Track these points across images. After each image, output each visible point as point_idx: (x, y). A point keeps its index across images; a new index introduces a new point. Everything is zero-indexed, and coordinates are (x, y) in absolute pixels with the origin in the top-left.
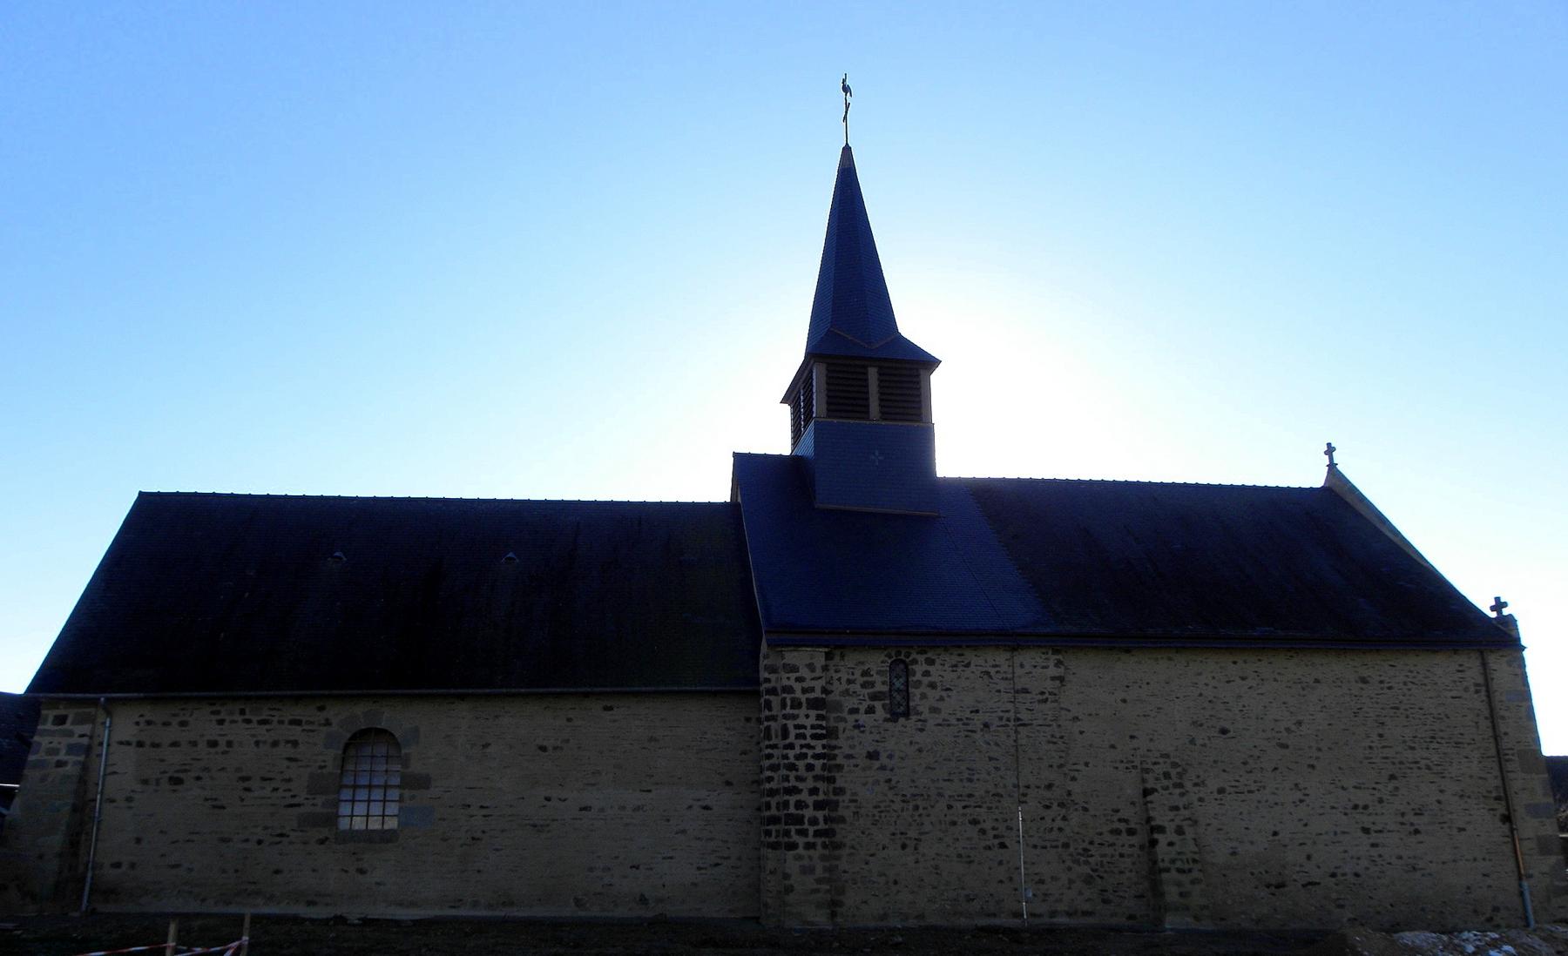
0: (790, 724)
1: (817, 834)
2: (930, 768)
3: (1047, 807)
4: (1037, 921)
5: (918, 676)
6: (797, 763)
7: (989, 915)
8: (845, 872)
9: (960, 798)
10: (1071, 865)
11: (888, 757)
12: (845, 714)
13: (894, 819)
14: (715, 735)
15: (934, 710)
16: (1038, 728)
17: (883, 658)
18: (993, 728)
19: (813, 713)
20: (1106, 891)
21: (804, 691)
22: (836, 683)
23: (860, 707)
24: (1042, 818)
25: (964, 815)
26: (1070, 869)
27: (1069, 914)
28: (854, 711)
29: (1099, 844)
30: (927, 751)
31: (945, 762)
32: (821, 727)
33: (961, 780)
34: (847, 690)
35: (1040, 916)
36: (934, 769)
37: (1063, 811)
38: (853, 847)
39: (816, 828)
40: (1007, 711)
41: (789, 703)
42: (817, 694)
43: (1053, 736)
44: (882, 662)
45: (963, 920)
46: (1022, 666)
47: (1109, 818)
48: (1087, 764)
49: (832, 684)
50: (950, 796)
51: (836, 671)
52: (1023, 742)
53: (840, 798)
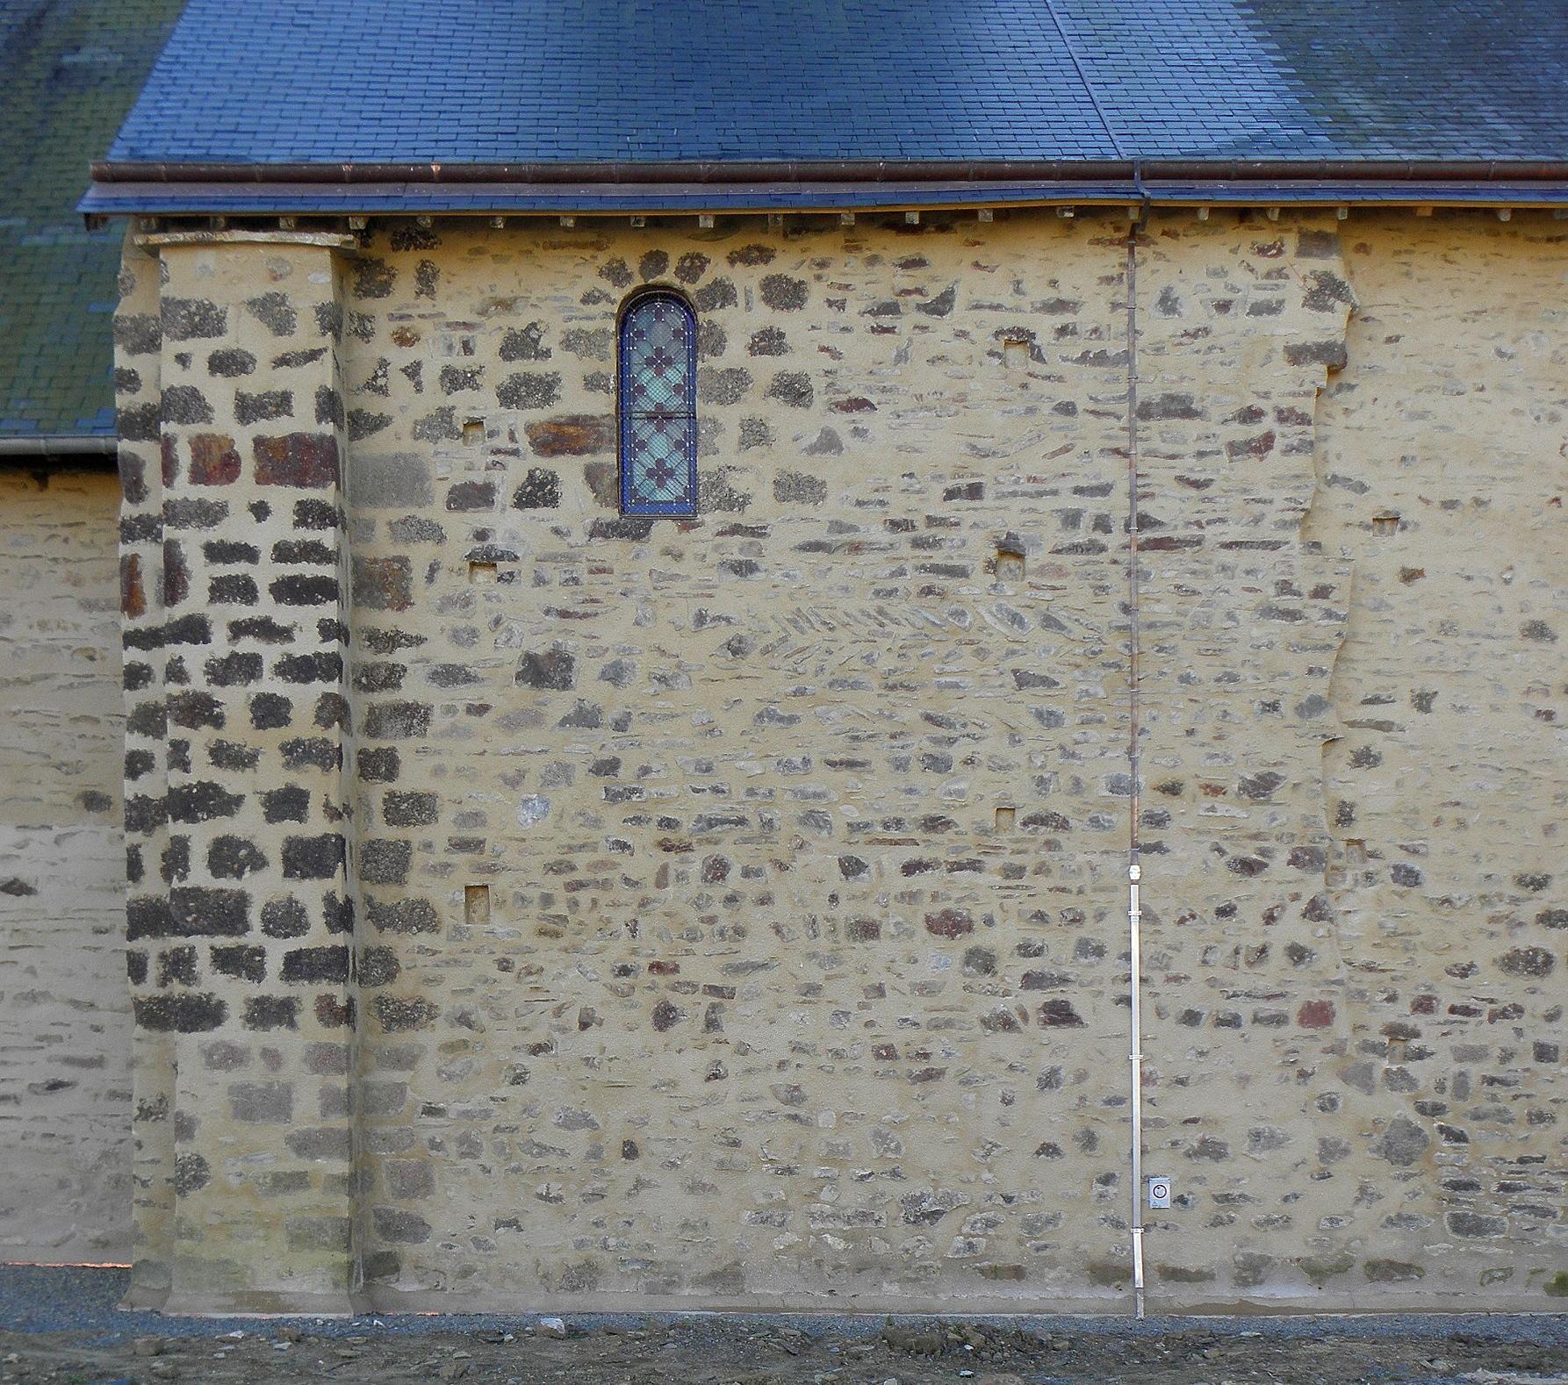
0: (191, 541)
1: (296, 966)
2: (772, 716)
3: (1249, 867)
4: (1185, 1296)
5: (735, 354)
6: (218, 693)
7: (994, 1273)
8: (431, 1111)
9: (894, 834)
10: (1334, 1085)
11: (604, 676)
12: (436, 511)
13: (627, 914)
14: (43, 625)
15: (795, 488)
16: (1228, 556)
17: (591, 280)
18: (1034, 559)
19: (283, 498)
20: (1470, 1186)
21: (247, 409)
22: (399, 384)
23: (496, 477)
24: (1225, 912)
25: (911, 897)
26: (1329, 1104)
27: (1316, 1273)
28: (473, 496)
29: (1453, 1010)
30: (765, 651)
31: (832, 694)
32: (313, 552)
33: (901, 765)
34: (446, 414)
35: (1199, 1277)
36: (792, 720)
37: (1314, 885)
38: (464, 1020)
39: (294, 944)
40: (1104, 490)
41: (184, 455)
42: (303, 421)
43: (1285, 588)
44: (588, 299)
45: (891, 1289)
46: (1168, 303)
47: (1503, 908)
48: (1423, 702)
49: (383, 391)
50: (854, 827)
51: (403, 339)
52: (1162, 610)
53: (415, 834)
